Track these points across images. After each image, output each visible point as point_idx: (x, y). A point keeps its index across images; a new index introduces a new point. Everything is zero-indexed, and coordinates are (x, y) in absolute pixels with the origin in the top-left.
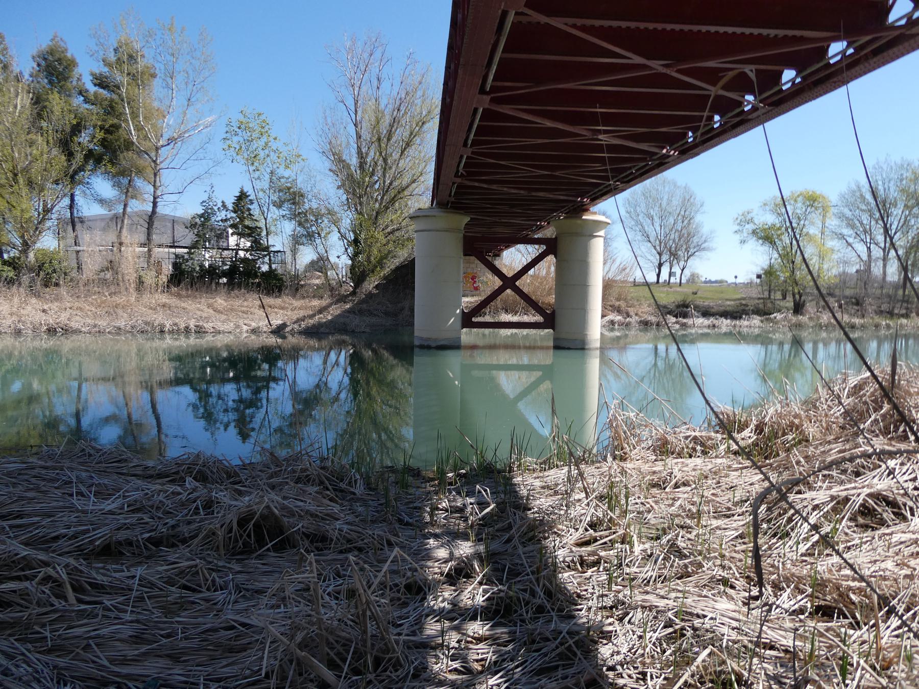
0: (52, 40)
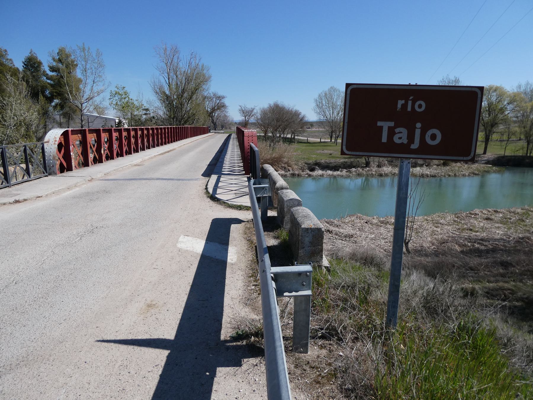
0: (30, 53)
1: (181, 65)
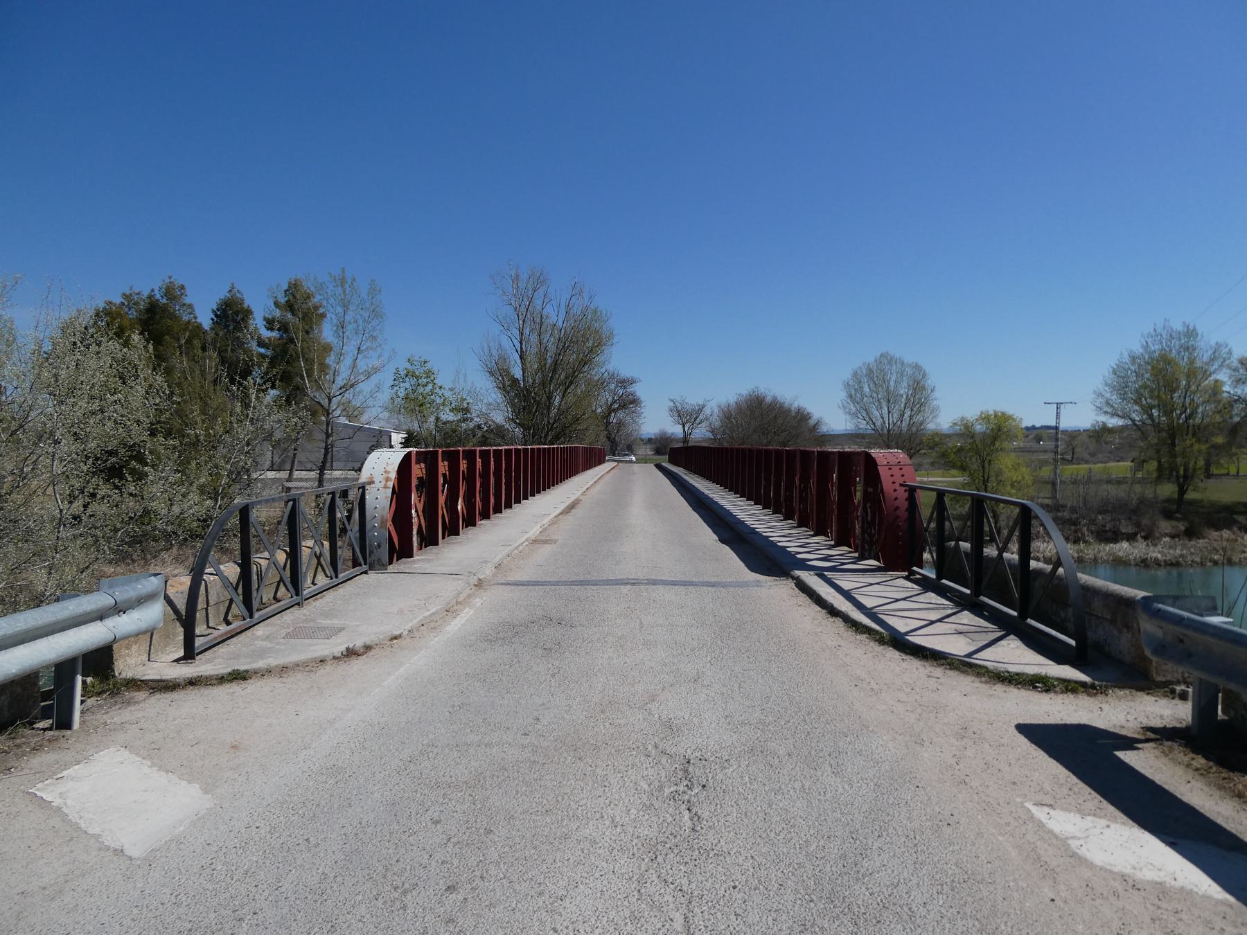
0: (230, 291)
1: (548, 310)
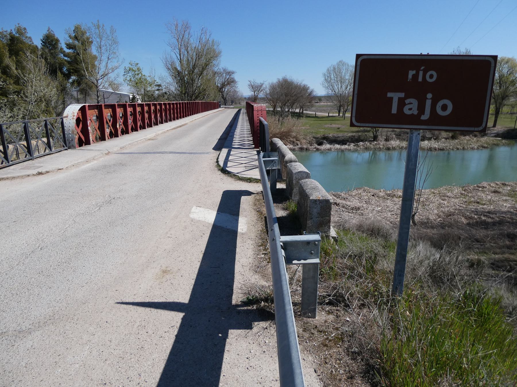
0: (48, 31)
